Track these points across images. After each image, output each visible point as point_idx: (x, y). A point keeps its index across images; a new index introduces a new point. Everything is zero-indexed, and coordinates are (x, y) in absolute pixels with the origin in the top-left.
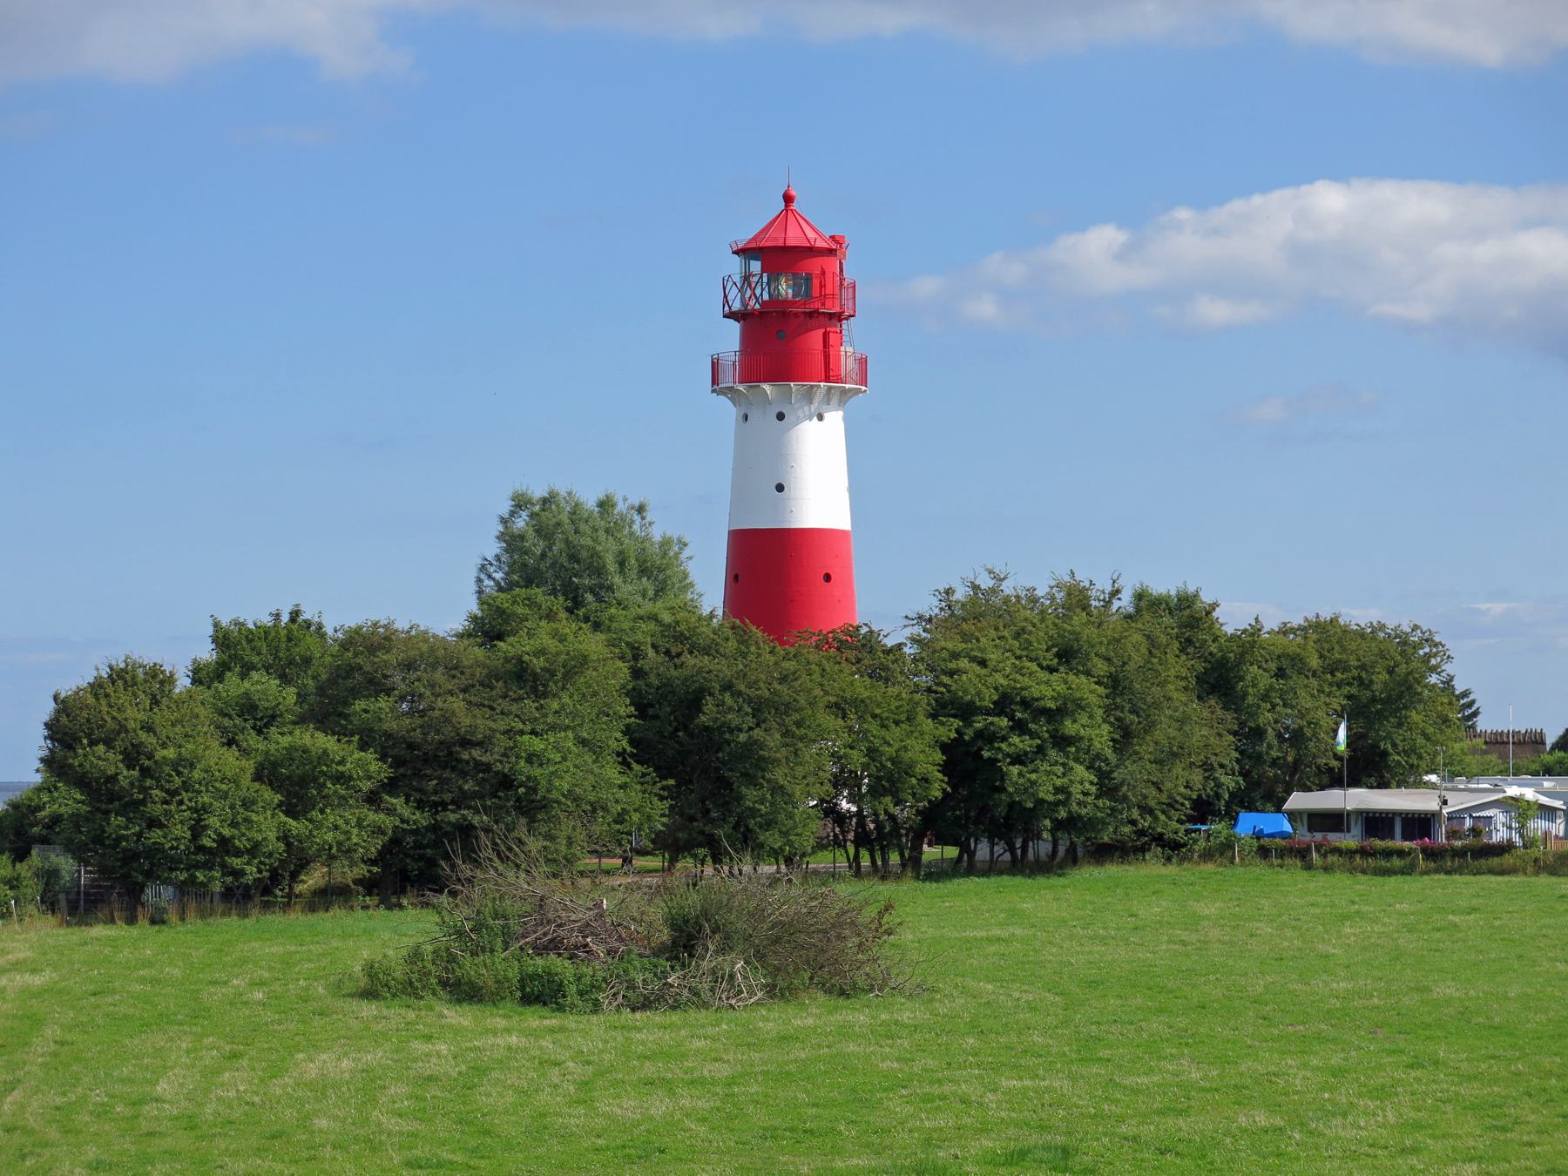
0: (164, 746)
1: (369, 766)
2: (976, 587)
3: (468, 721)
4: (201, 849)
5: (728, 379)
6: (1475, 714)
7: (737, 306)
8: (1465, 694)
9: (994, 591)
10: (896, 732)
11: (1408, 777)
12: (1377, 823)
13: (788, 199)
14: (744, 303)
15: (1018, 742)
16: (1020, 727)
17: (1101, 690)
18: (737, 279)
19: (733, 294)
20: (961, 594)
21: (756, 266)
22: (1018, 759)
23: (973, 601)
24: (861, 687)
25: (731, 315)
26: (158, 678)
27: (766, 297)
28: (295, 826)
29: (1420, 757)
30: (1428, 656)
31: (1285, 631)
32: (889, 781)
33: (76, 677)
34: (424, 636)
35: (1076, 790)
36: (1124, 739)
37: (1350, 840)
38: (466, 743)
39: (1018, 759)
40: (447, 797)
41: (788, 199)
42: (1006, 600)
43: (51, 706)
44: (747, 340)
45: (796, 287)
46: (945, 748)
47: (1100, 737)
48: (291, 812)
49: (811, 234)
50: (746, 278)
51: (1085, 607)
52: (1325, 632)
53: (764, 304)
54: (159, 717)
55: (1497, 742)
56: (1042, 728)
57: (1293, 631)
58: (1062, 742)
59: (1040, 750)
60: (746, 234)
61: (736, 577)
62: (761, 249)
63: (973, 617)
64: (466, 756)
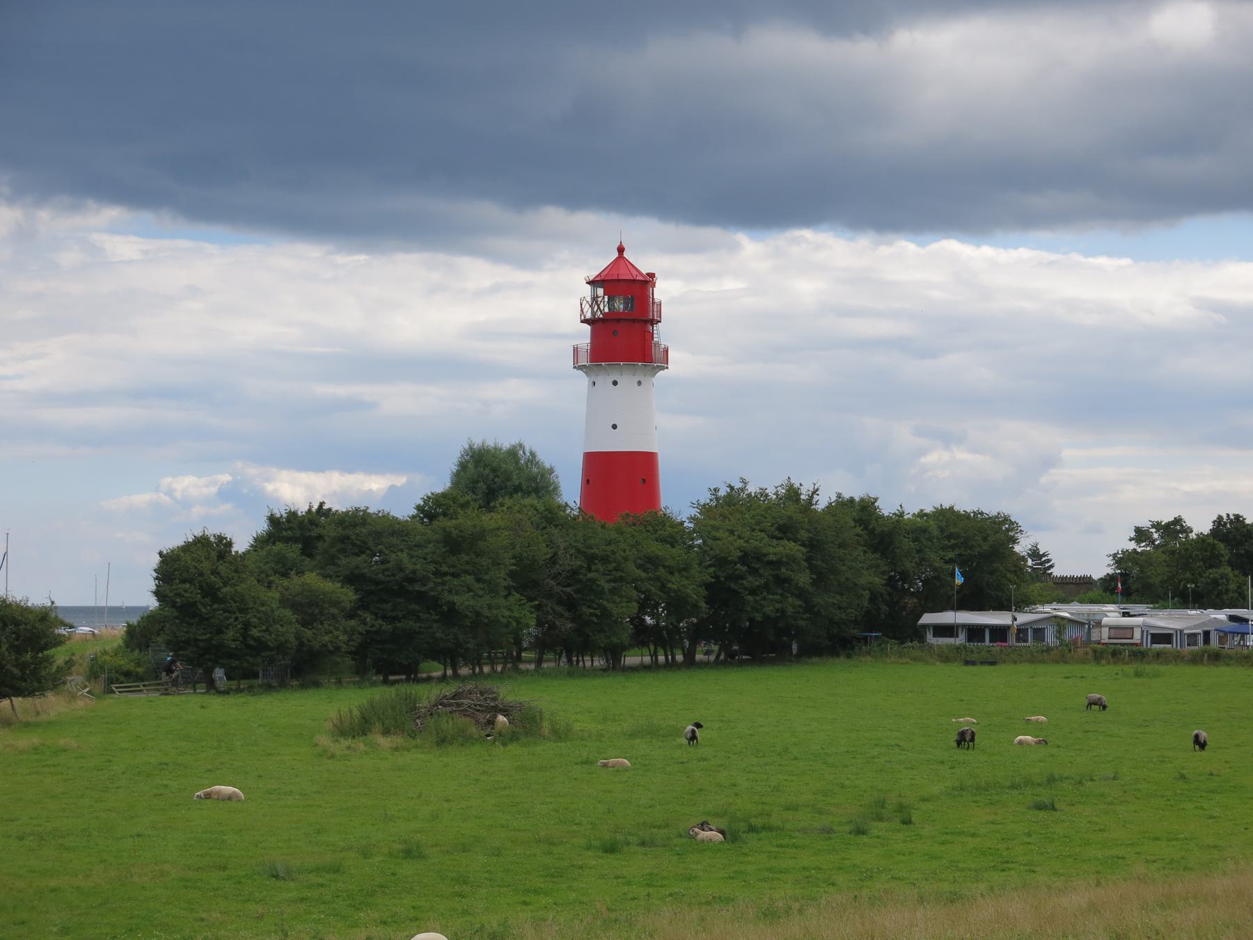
0: (225, 584)
1: (348, 595)
2: (732, 488)
3: (411, 567)
4: (248, 646)
5: (584, 360)
6: (1052, 566)
7: (589, 316)
8: (1044, 555)
9: (742, 490)
10: (676, 578)
11: (1022, 604)
12: (975, 632)
13: (621, 250)
14: (593, 313)
15: (752, 581)
16: (754, 572)
17: (804, 550)
18: (589, 299)
19: (587, 308)
20: (722, 493)
21: (600, 291)
22: (753, 592)
23: (729, 495)
24: (656, 549)
25: (585, 321)
26: (224, 544)
27: (606, 310)
28: (309, 633)
29: (506, 597)
30: (1008, 530)
31: (922, 514)
32: (678, 606)
33: (175, 541)
34: (386, 517)
35: (790, 610)
36: (820, 580)
37: (961, 639)
38: (411, 580)
39: (753, 592)
40: (400, 614)
41: (621, 250)
42: (749, 495)
43: (157, 559)
44: (594, 335)
45: (626, 304)
46: (708, 586)
47: (804, 579)
48: (304, 624)
49: (634, 273)
50: (595, 298)
51: (798, 500)
52: (946, 516)
53: (605, 314)
54: (222, 568)
55: (1065, 582)
56: (767, 573)
57: (926, 515)
58: (781, 581)
59: (766, 587)
60: (593, 275)
61: (588, 481)
62: (603, 281)
63: (731, 507)
64: (411, 588)
